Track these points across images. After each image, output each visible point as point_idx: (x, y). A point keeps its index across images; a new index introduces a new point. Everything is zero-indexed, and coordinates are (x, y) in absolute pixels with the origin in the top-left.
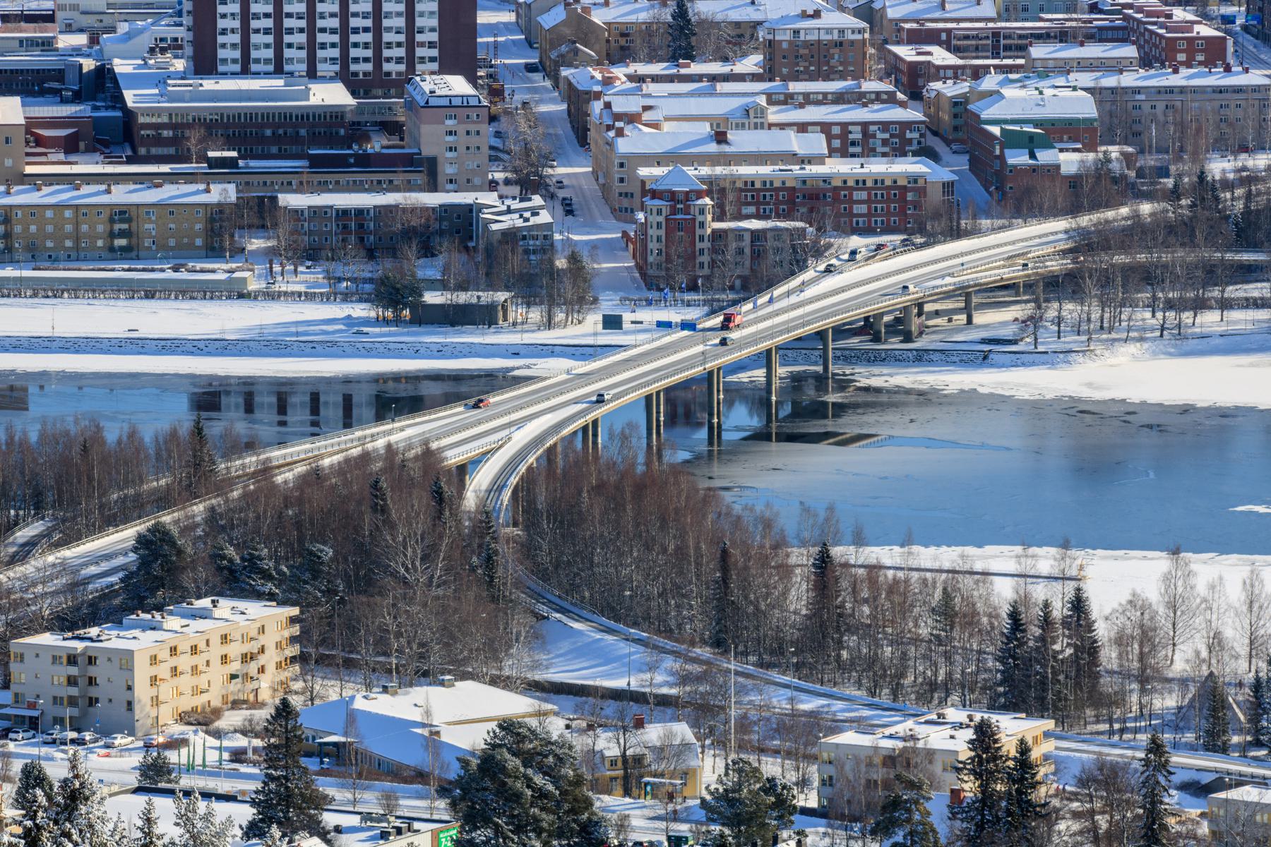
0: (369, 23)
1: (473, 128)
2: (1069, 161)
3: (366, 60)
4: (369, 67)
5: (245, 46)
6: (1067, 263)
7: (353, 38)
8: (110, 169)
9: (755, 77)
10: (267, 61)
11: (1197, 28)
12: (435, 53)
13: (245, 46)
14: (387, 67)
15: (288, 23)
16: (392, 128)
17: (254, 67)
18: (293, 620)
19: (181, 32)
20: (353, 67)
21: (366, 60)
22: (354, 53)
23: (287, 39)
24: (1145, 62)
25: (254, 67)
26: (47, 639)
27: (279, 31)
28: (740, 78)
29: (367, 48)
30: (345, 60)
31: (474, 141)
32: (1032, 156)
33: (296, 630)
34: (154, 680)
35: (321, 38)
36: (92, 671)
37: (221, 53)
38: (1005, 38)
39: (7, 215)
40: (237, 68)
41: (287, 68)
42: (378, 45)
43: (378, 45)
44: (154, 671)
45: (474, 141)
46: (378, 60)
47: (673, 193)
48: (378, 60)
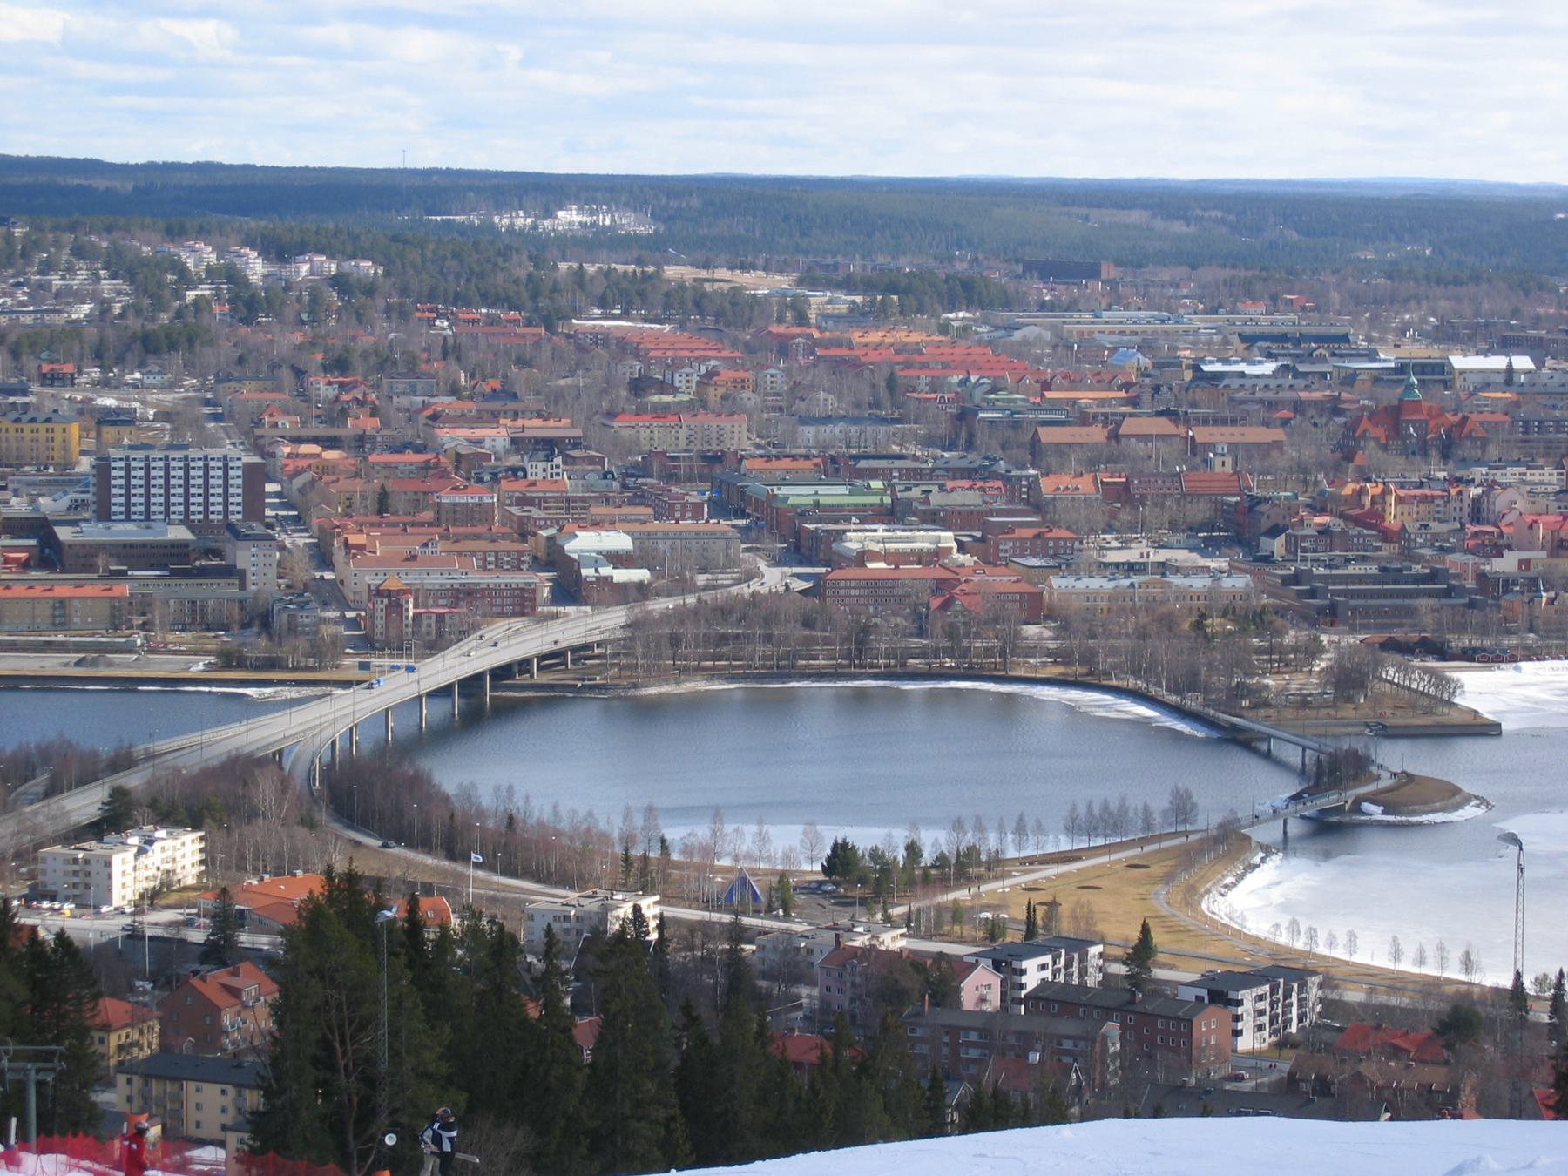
0: (201, 491)
1: (268, 552)
2: (621, 575)
3: (200, 513)
4: (201, 517)
5: (128, 504)
6: (628, 633)
7: (172, 491)
8: (52, 576)
9: (430, 524)
10: (141, 513)
11: (686, 498)
12: (240, 509)
13: (128, 504)
14: (212, 517)
15: (153, 491)
16: (218, 553)
17: (133, 517)
18: (201, 839)
19: (89, 497)
20: (192, 517)
21: (200, 513)
22: (133, 482)
23: (153, 500)
24: (658, 517)
25: (133, 517)
26: (57, 848)
27: (148, 495)
28: (422, 524)
29: (53, 430)
30: (187, 512)
31: (268, 560)
32: (597, 571)
33: (202, 856)
34: (124, 873)
35: (133, 482)
36: (88, 868)
37: (114, 509)
38: (561, 508)
39: (1567, 361)
40: (123, 517)
41: (152, 517)
42: (206, 504)
43: (206, 504)
44: (124, 868)
45: (268, 560)
46: (206, 512)
47: (389, 591)
48: (206, 512)
